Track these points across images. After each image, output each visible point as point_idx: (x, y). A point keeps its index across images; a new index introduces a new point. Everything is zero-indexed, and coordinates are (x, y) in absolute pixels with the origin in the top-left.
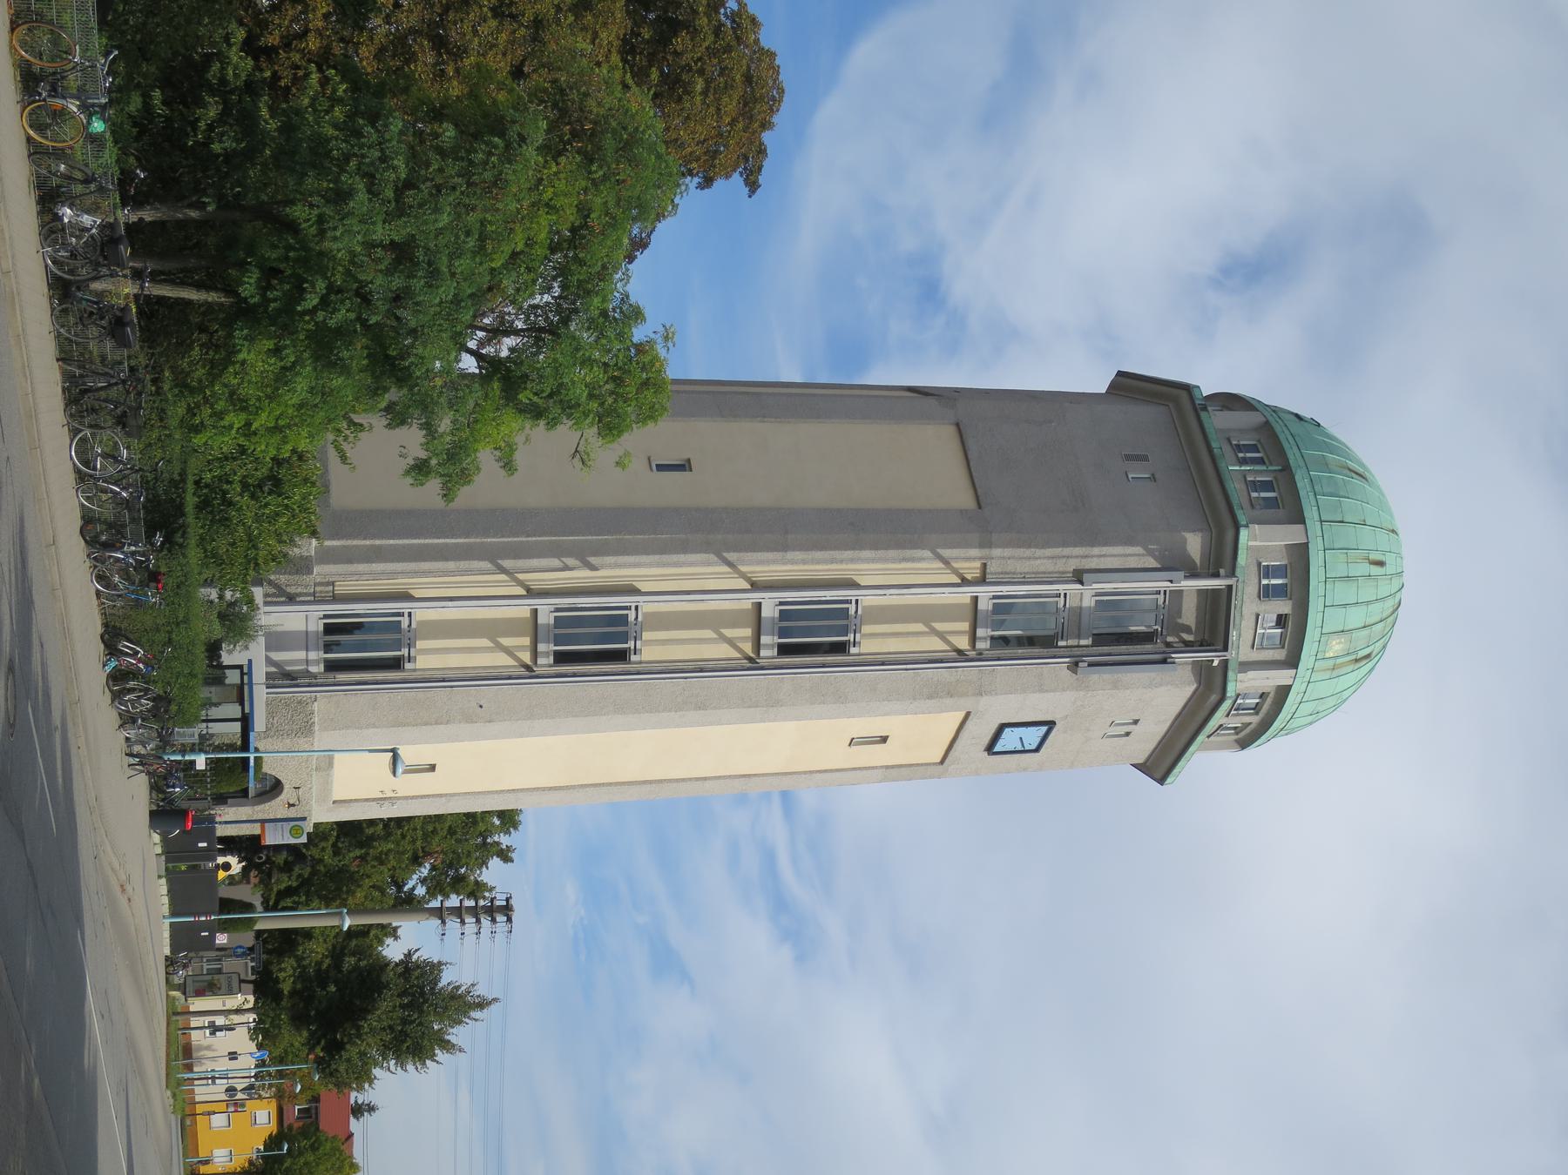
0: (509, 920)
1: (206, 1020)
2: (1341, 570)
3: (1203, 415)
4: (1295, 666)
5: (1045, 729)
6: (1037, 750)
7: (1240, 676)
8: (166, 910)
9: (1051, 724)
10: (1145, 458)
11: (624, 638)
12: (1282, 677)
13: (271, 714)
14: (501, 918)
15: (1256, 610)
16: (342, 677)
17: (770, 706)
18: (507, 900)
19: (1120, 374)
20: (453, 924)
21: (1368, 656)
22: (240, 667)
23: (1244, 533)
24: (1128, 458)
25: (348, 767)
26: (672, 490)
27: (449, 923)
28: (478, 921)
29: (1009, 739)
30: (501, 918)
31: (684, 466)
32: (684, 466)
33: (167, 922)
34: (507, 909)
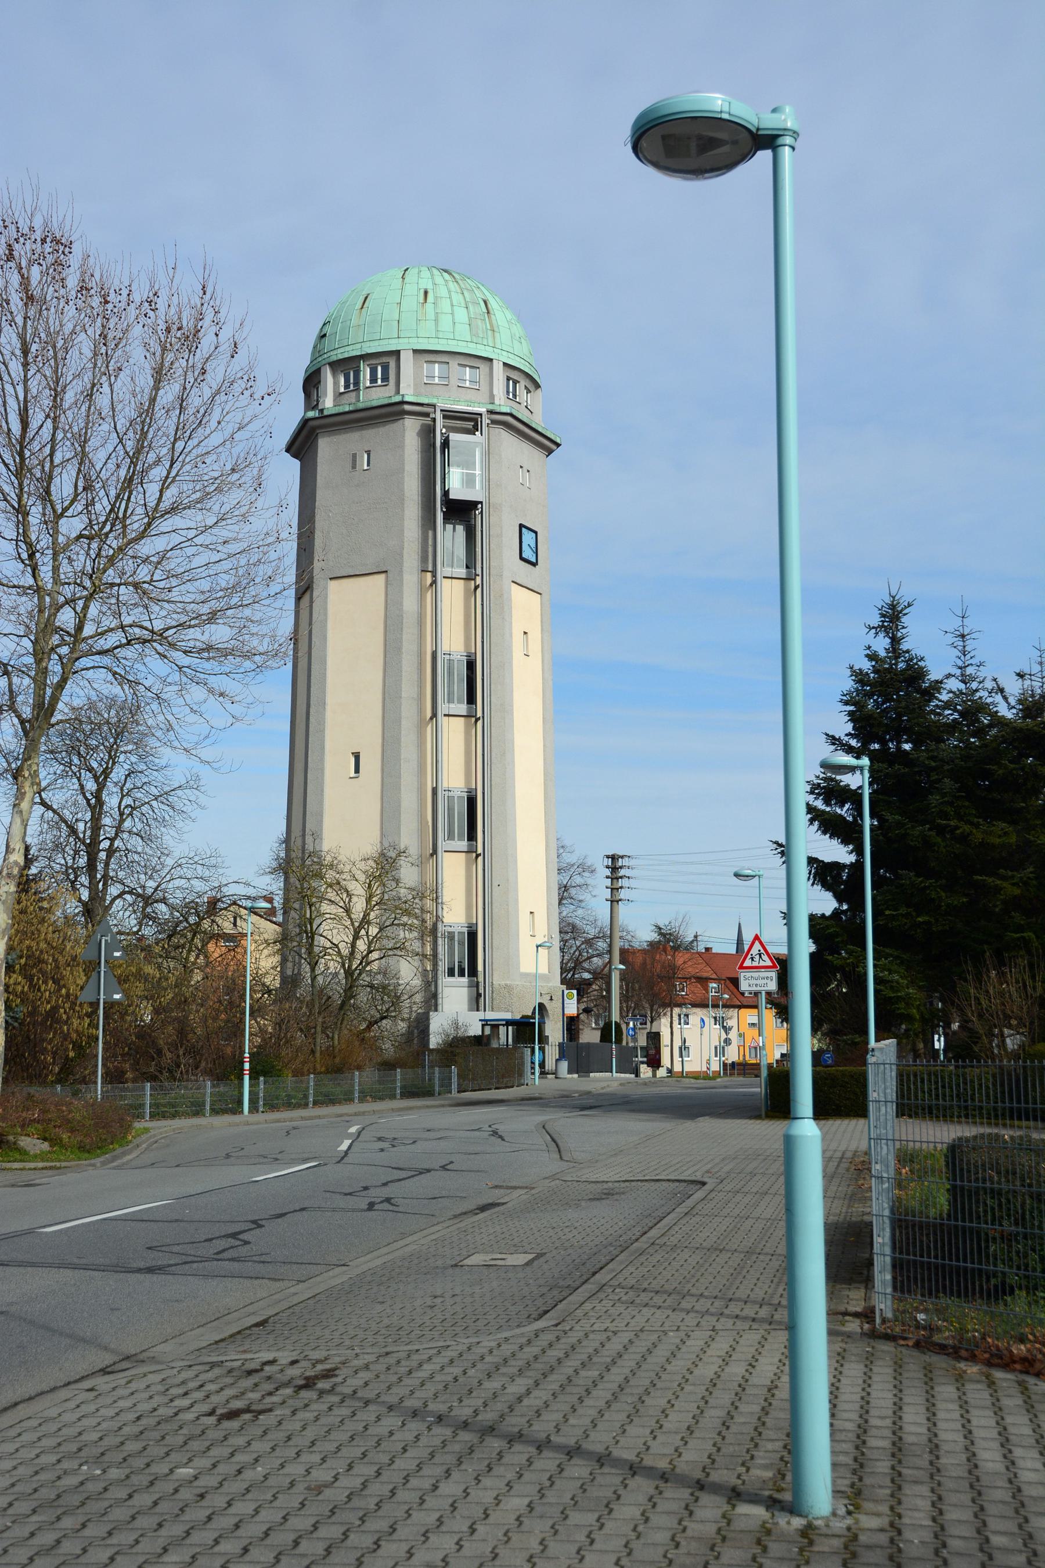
0: (622, 857)
1: (677, 1059)
2: (431, 324)
3: (326, 413)
4: (491, 360)
5: (524, 529)
6: (536, 533)
7: (497, 402)
8: (609, 1074)
9: (521, 526)
10: (354, 456)
11: (966, 1296)
12: (498, 367)
13: (499, 1010)
14: (620, 863)
15: (455, 387)
16: (480, 968)
17: (507, 709)
18: (608, 857)
19: (288, 450)
20: (623, 894)
21: (485, 302)
22: (483, 1026)
23: (407, 399)
24: (354, 467)
25: (529, 964)
26: (371, 764)
27: (622, 896)
28: (621, 867)
29: (528, 554)
30: (620, 863)
31: (357, 757)
32: (357, 757)
33: (615, 1074)
34: (614, 858)
